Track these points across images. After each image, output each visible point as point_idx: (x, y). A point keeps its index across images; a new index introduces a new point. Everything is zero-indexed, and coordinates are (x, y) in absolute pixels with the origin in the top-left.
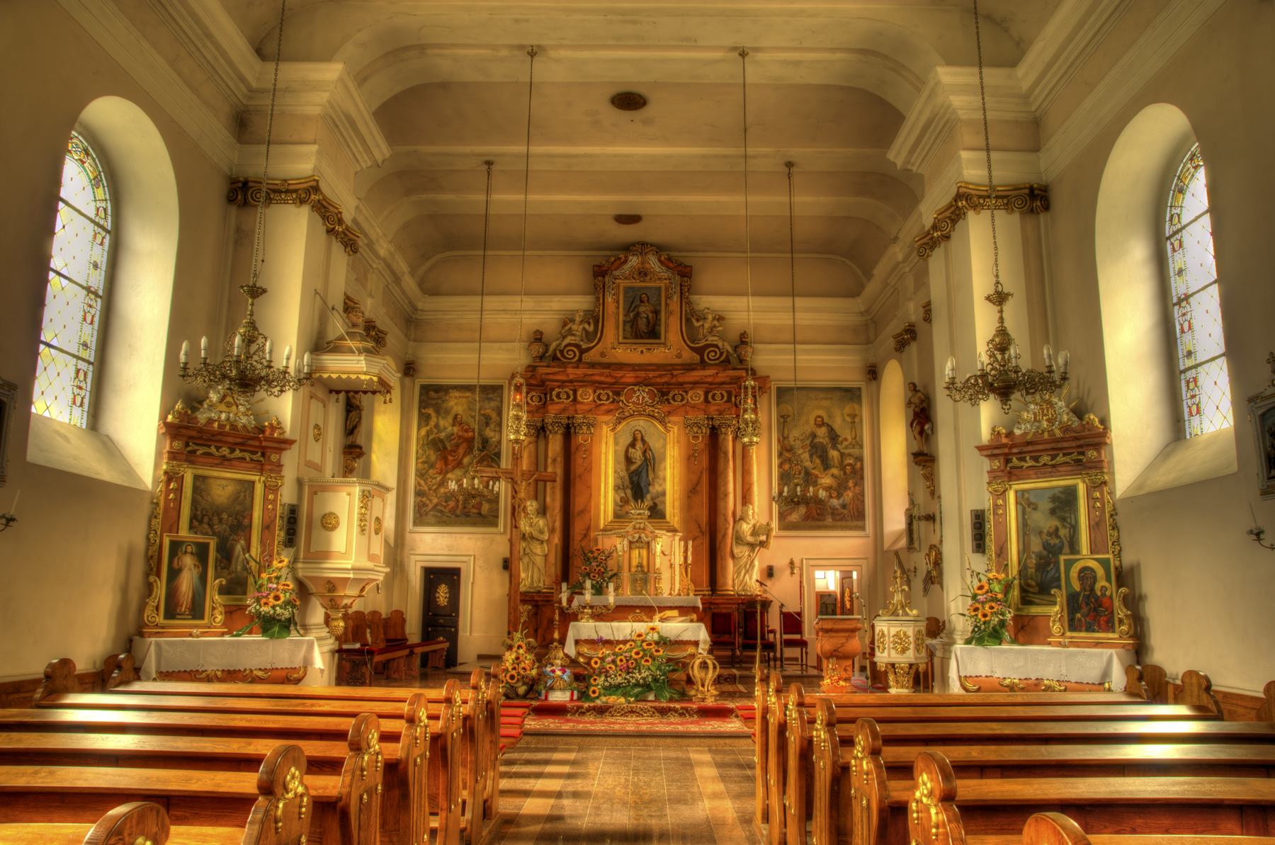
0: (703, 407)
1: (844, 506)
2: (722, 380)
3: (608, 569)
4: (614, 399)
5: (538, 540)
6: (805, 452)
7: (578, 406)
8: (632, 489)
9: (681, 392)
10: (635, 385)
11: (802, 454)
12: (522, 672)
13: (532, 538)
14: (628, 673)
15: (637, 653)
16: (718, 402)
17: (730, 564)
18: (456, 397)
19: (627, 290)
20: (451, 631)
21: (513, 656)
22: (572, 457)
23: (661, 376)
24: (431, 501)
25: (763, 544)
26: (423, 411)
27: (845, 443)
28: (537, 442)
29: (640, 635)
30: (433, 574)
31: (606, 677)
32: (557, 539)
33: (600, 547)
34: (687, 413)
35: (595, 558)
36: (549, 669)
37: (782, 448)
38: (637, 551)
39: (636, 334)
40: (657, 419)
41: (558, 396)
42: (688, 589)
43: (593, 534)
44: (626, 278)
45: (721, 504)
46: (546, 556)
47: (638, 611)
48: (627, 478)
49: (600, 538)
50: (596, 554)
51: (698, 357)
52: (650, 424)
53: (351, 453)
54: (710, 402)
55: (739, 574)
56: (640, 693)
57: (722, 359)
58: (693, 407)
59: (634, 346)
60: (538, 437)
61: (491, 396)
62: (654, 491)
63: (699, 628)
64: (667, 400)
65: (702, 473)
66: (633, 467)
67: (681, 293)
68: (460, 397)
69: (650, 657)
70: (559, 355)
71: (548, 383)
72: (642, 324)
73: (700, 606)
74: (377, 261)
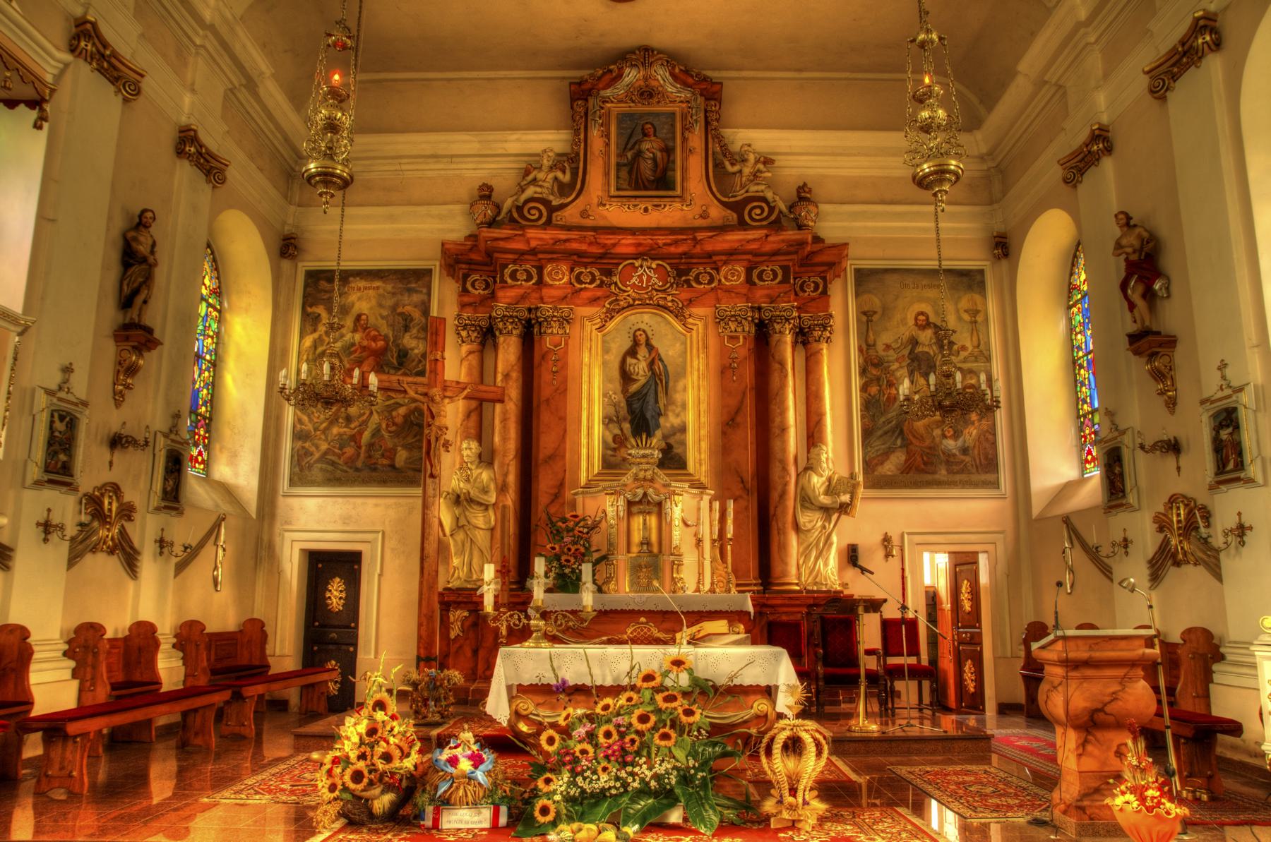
0: (744, 291)
1: (965, 451)
2: (775, 246)
3: (593, 549)
4: (602, 282)
5: (480, 504)
6: (901, 367)
7: (545, 292)
8: (631, 422)
9: (709, 270)
10: (636, 259)
11: (897, 369)
12: (381, 765)
13: (471, 501)
14: (624, 764)
15: (643, 719)
16: (769, 284)
17: (793, 540)
18: (359, 289)
19: (622, 118)
20: (349, 651)
21: (362, 728)
22: (536, 372)
23: (676, 243)
24: (317, 447)
25: (844, 509)
26: (309, 310)
27: (963, 354)
28: (481, 352)
29: (649, 678)
30: (322, 562)
31: (574, 773)
32: (510, 500)
33: (579, 512)
34: (718, 300)
35: (569, 530)
36: (446, 754)
37: (865, 361)
38: (641, 519)
39: (637, 182)
40: (671, 312)
41: (513, 275)
42: (729, 582)
43: (568, 494)
44: (620, 101)
45: (776, 444)
46: (492, 530)
47: (643, 619)
48: (623, 404)
49: (579, 499)
50: (571, 524)
51: (735, 216)
52: (659, 319)
53: (127, 339)
54: (755, 284)
55: (807, 557)
56: (651, 811)
57: (773, 217)
58: (728, 291)
59: (634, 202)
60: (483, 344)
61: (413, 285)
62: (668, 425)
63: (777, 658)
64: (687, 282)
65: (744, 394)
66: (634, 388)
67: (707, 123)
68: (365, 288)
69: (673, 726)
70: (516, 215)
71: (496, 255)
72: (646, 168)
73: (751, 609)
74: (201, 32)
